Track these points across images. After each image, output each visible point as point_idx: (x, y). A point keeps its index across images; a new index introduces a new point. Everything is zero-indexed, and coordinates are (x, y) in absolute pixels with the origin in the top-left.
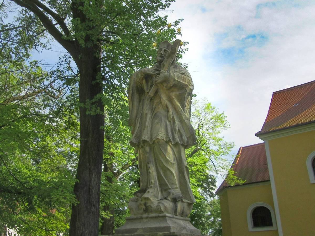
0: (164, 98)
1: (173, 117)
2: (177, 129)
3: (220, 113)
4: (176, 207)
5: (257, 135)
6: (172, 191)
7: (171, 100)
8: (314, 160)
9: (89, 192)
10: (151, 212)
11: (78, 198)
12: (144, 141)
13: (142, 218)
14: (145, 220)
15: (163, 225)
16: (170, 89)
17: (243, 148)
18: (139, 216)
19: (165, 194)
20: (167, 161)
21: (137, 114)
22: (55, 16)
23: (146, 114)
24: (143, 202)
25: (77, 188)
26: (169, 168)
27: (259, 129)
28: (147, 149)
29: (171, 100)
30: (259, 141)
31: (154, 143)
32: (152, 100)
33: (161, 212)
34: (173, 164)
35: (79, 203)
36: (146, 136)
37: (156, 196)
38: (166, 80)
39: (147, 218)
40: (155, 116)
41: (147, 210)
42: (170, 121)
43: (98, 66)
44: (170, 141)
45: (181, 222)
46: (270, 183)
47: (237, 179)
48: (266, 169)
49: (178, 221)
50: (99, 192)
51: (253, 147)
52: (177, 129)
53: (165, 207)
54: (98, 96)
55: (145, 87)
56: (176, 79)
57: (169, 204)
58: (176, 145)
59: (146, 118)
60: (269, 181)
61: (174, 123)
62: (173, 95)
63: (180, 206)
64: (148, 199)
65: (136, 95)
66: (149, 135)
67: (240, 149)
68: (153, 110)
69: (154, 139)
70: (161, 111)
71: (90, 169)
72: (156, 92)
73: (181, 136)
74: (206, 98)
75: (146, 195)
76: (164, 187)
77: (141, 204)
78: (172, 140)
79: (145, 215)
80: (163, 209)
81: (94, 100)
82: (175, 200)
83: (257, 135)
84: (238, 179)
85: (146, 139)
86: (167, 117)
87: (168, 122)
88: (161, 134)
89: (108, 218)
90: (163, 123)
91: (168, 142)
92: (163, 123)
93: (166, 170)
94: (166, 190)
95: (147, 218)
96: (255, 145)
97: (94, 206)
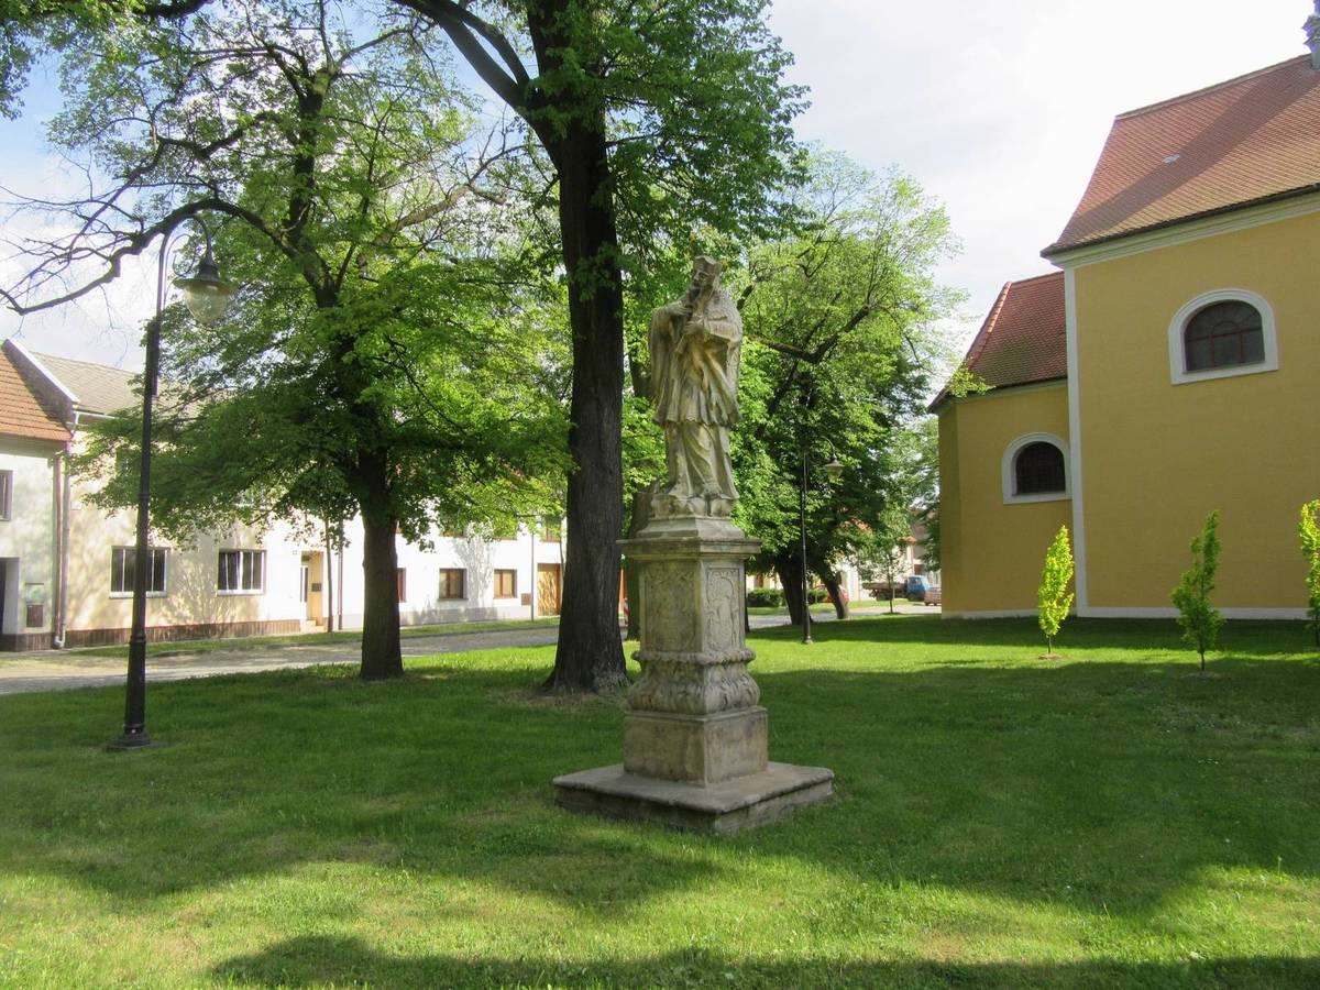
0: (697, 357)
1: (709, 388)
2: (714, 404)
3: (938, 207)
4: (709, 506)
5: (1046, 254)
6: (706, 486)
7: (706, 360)
8: (1192, 320)
9: (600, 445)
10: (679, 513)
11: (577, 459)
12: (670, 422)
13: (668, 520)
14: (671, 522)
15: (691, 528)
16: (706, 346)
17: (1013, 284)
18: (664, 517)
19: (698, 489)
20: (700, 448)
21: (662, 376)
22: (487, 30)
23: (673, 381)
24: (669, 501)
25: (573, 437)
26: (703, 456)
27: (1053, 237)
28: (675, 431)
29: (706, 360)
30: (1047, 268)
31: (682, 423)
32: (681, 357)
33: (690, 513)
34: (708, 451)
35: (579, 468)
36: (672, 416)
37: (685, 493)
38: (699, 332)
39: (673, 519)
40: (685, 384)
41: (674, 510)
42: (705, 392)
43: (599, 163)
44: (703, 422)
45: (717, 523)
46: (1067, 383)
47: (970, 380)
48: (1061, 347)
49: (712, 523)
50: (620, 440)
51: (1041, 281)
52: (714, 404)
53: (695, 509)
54: (604, 248)
55: (672, 334)
56: (712, 333)
57: (700, 503)
58: (712, 425)
59: (673, 385)
60: (1066, 377)
61: (710, 393)
62: (709, 354)
63: (714, 505)
64: (674, 497)
65: (660, 345)
66: (676, 413)
67: (1005, 288)
68: (682, 373)
69: (682, 419)
70: (693, 376)
71: (598, 400)
72: (686, 349)
73: (720, 412)
74: (895, 166)
75: (672, 493)
76: (697, 482)
77: (666, 504)
78: (705, 420)
79: (671, 517)
80: (691, 509)
81: (598, 259)
82: (709, 499)
83: (1046, 254)
84: (975, 380)
85: (672, 419)
86: (701, 386)
87: (701, 394)
88: (691, 414)
89: (646, 484)
90: (695, 396)
91: (701, 423)
92: (695, 396)
93: (699, 459)
94: (699, 485)
95: (673, 519)
96: (1029, 280)
97: (611, 472)
